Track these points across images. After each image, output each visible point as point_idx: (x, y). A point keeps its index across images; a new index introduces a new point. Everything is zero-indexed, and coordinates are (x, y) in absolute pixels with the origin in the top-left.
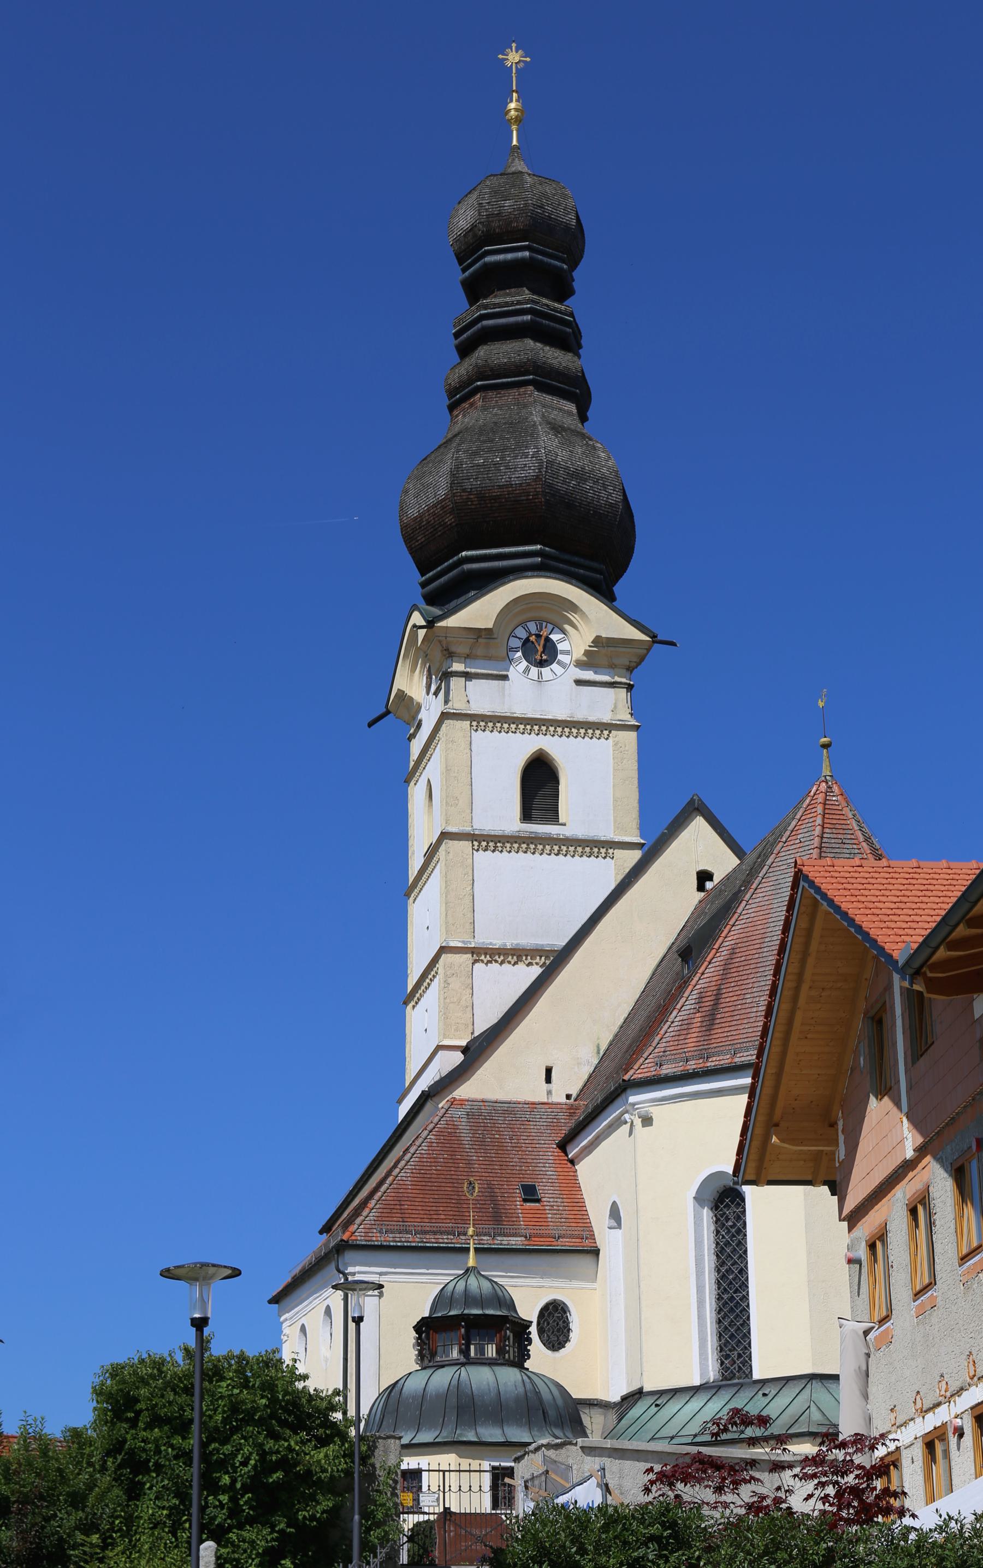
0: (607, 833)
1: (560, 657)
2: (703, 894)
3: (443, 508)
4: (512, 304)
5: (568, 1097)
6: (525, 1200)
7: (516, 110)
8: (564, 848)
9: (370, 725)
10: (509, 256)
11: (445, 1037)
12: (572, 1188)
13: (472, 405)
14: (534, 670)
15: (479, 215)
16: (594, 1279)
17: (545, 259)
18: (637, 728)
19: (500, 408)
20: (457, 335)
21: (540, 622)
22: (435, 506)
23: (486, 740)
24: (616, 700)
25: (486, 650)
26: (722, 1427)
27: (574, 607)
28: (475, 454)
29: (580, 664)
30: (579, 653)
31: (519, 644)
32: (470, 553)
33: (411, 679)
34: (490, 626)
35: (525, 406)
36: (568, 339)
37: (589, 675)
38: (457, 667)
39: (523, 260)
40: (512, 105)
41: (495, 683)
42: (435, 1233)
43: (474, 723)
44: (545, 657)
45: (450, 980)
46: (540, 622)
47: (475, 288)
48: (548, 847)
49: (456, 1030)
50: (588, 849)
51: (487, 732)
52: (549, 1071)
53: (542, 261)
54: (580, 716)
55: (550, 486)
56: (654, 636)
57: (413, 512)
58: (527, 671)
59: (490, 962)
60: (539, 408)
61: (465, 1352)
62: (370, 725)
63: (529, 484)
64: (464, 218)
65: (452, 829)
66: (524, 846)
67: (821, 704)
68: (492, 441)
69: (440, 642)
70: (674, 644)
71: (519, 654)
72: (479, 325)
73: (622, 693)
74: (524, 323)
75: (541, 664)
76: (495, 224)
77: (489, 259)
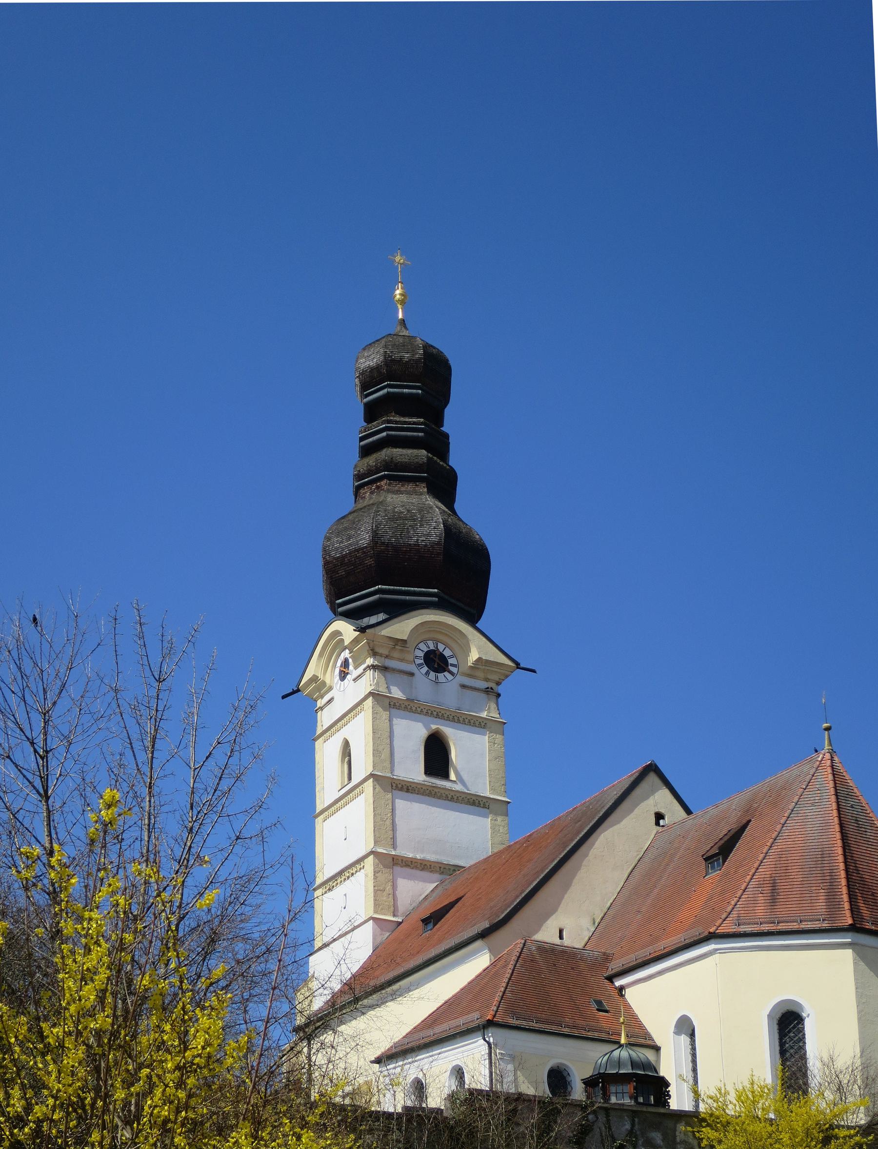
2: (660, 829)
4: (410, 423)
7: (400, 294)
9: (283, 697)
14: (432, 675)
20: (362, 439)
26: (170, 1125)
34: (405, 638)
36: (438, 444)
40: (398, 292)
41: (405, 677)
56: (518, 665)
58: (427, 673)
62: (283, 697)
70: (534, 671)
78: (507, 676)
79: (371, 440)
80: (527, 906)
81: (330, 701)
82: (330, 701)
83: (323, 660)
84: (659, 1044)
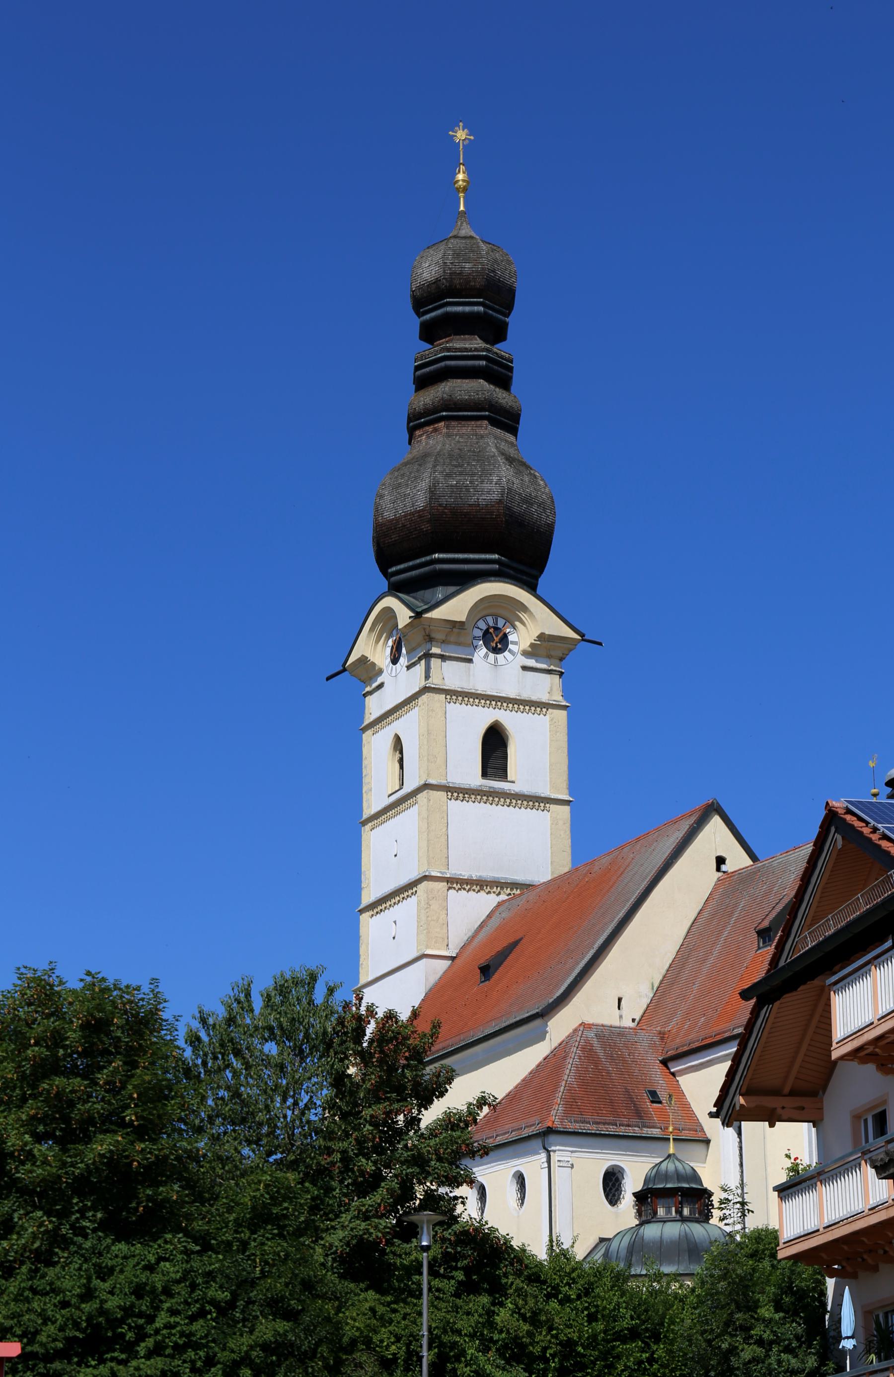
0: (545, 791)
1: (510, 646)
2: (720, 874)
3: (420, 517)
5: (633, 1020)
6: (652, 1102)
7: (464, 181)
8: (514, 801)
9: (328, 679)
10: (467, 309)
11: (427, 947)
12: (677, 1094)
13: (435, 430)
14: (492, 656)
15: (444, 271)
16: (705, 1162)
17: (494, 314)
18: (565, 708)
19: (461, 436)
20: (417, 368)
21: (496, 617)
22: (412, 514)
23: (457, 710)
24: (552, 684)
25: (456, 639)
27: (524, 608)
28: (449, 476)
29: (526, 654)
30: (525, 644)
31: (480, 634)
32: (442, 556)
33: (375, 648)
34: (464, 619)
35: (482, 437)
36: (500, 374)
37: (531, 663)
38: (435, 650)
39: (478, 313)
40: (460, 176)
42: (604, 1124)
43: (448, 697)
44: (499, 646)
45: (431, 902)
46: (496, 617)
47: (429, 333)
48: (502, 800)
49: (436, 942)
50: (531, 803)
51: (457, 704)
52: (620, 1000)
53: (492, 316)
54: (525, 696)
55: (509, 508)
57: (389, 515)
59: (459, 889)
60: (493, 439)
61: (679, 1212)
62: (328, 679)
63: (493, 506)
64: (428, 269)
65: (432, 781)
66: (485, 798)
67: (871, 764)
68: (462, 466)
69: (424, 629)
70: (600, 644)
71: (481, 642)
72: (443, 364)
73: (556, 678)
74: (480, 367)
75: (496, 651)
76: (457, 282)
77: (449, 309)
78: (571, 650)
79: (427, 369)
80: (470, 934)
81: (381, 686)
82: (381, 686)
83: (374, 635)
84: (709, 1137)
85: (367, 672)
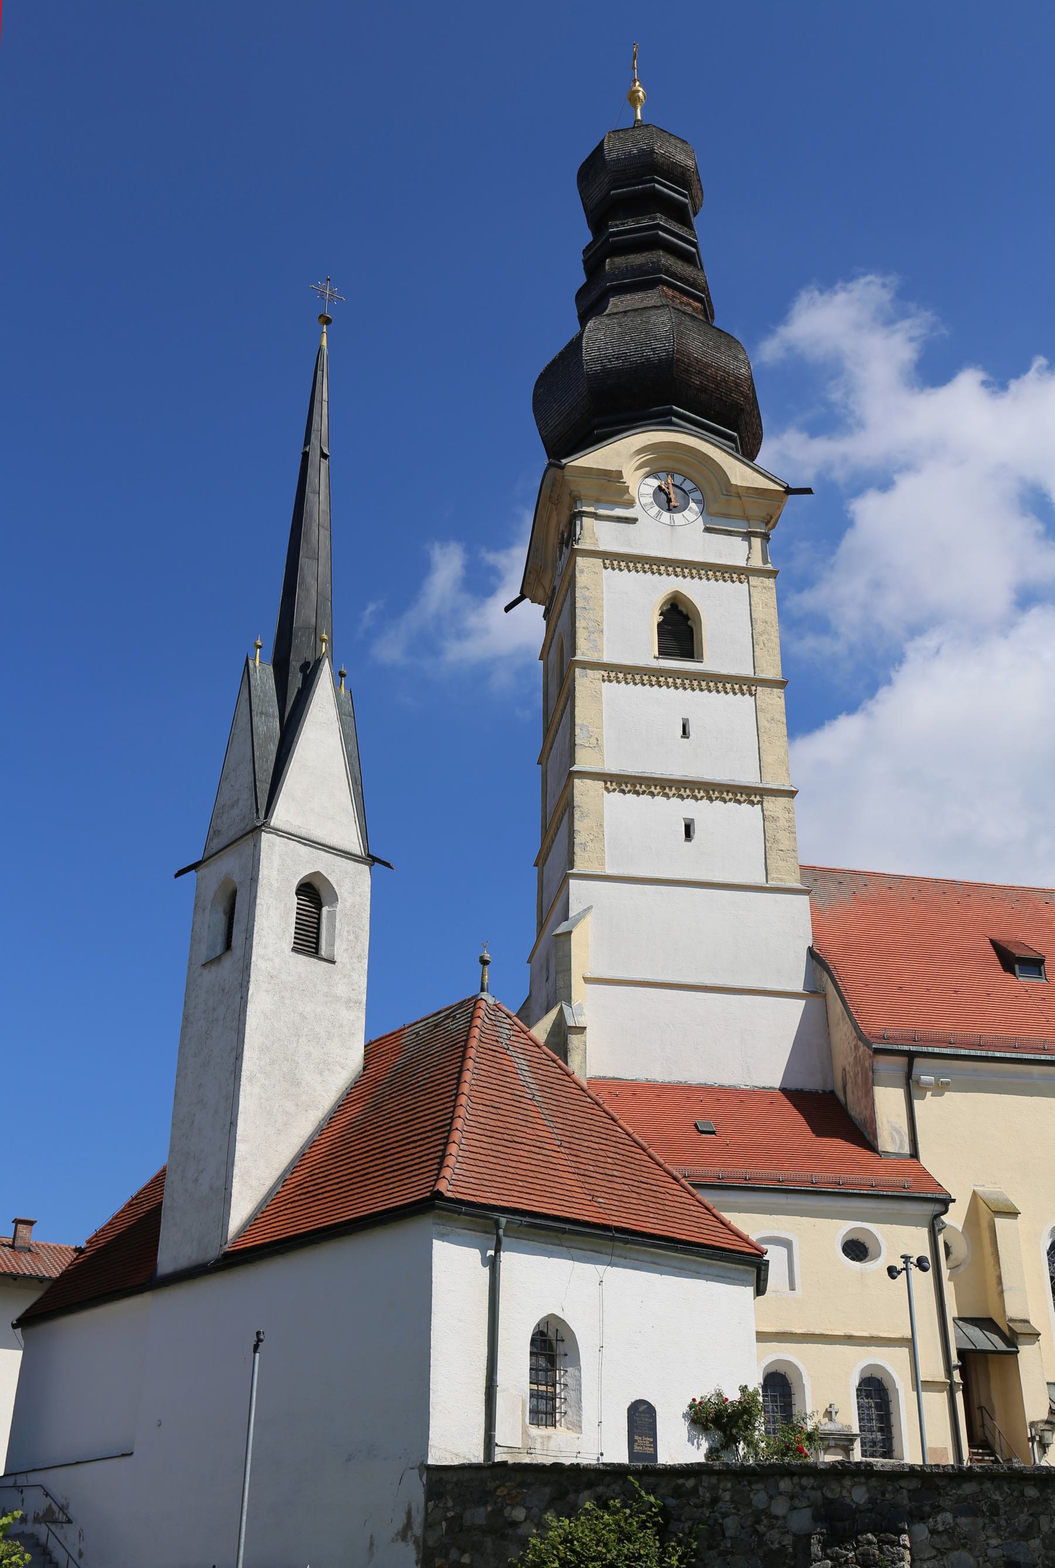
81: (633, 521)
82: (633, 521)
85: (611, 487)
